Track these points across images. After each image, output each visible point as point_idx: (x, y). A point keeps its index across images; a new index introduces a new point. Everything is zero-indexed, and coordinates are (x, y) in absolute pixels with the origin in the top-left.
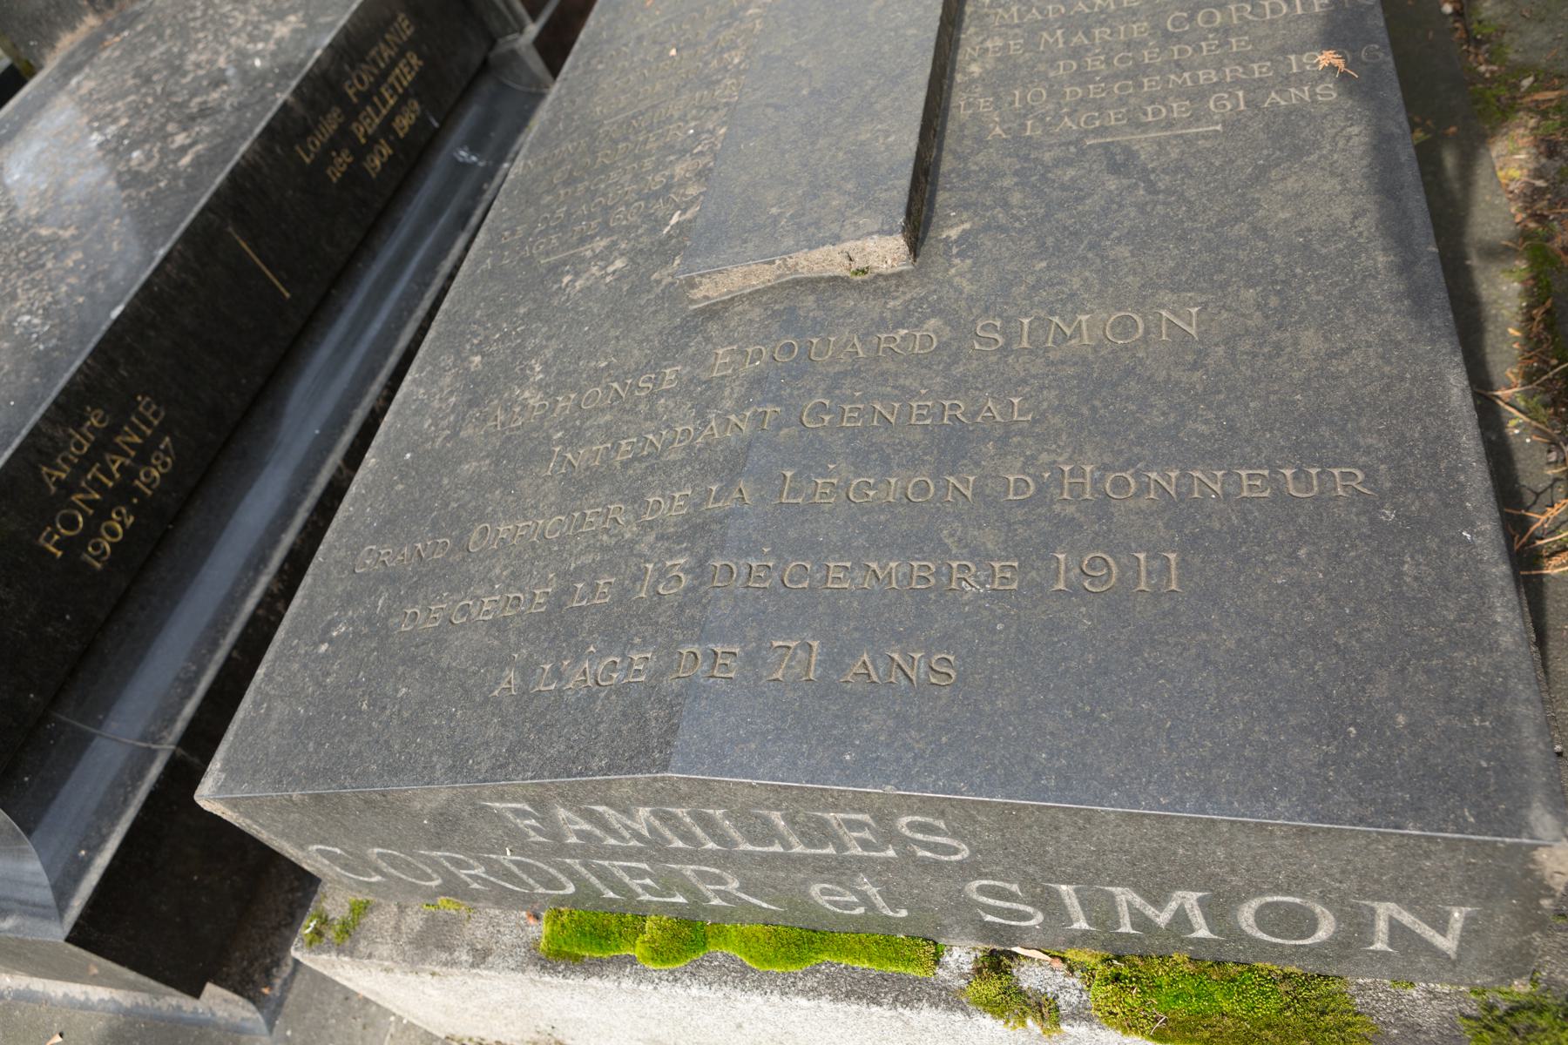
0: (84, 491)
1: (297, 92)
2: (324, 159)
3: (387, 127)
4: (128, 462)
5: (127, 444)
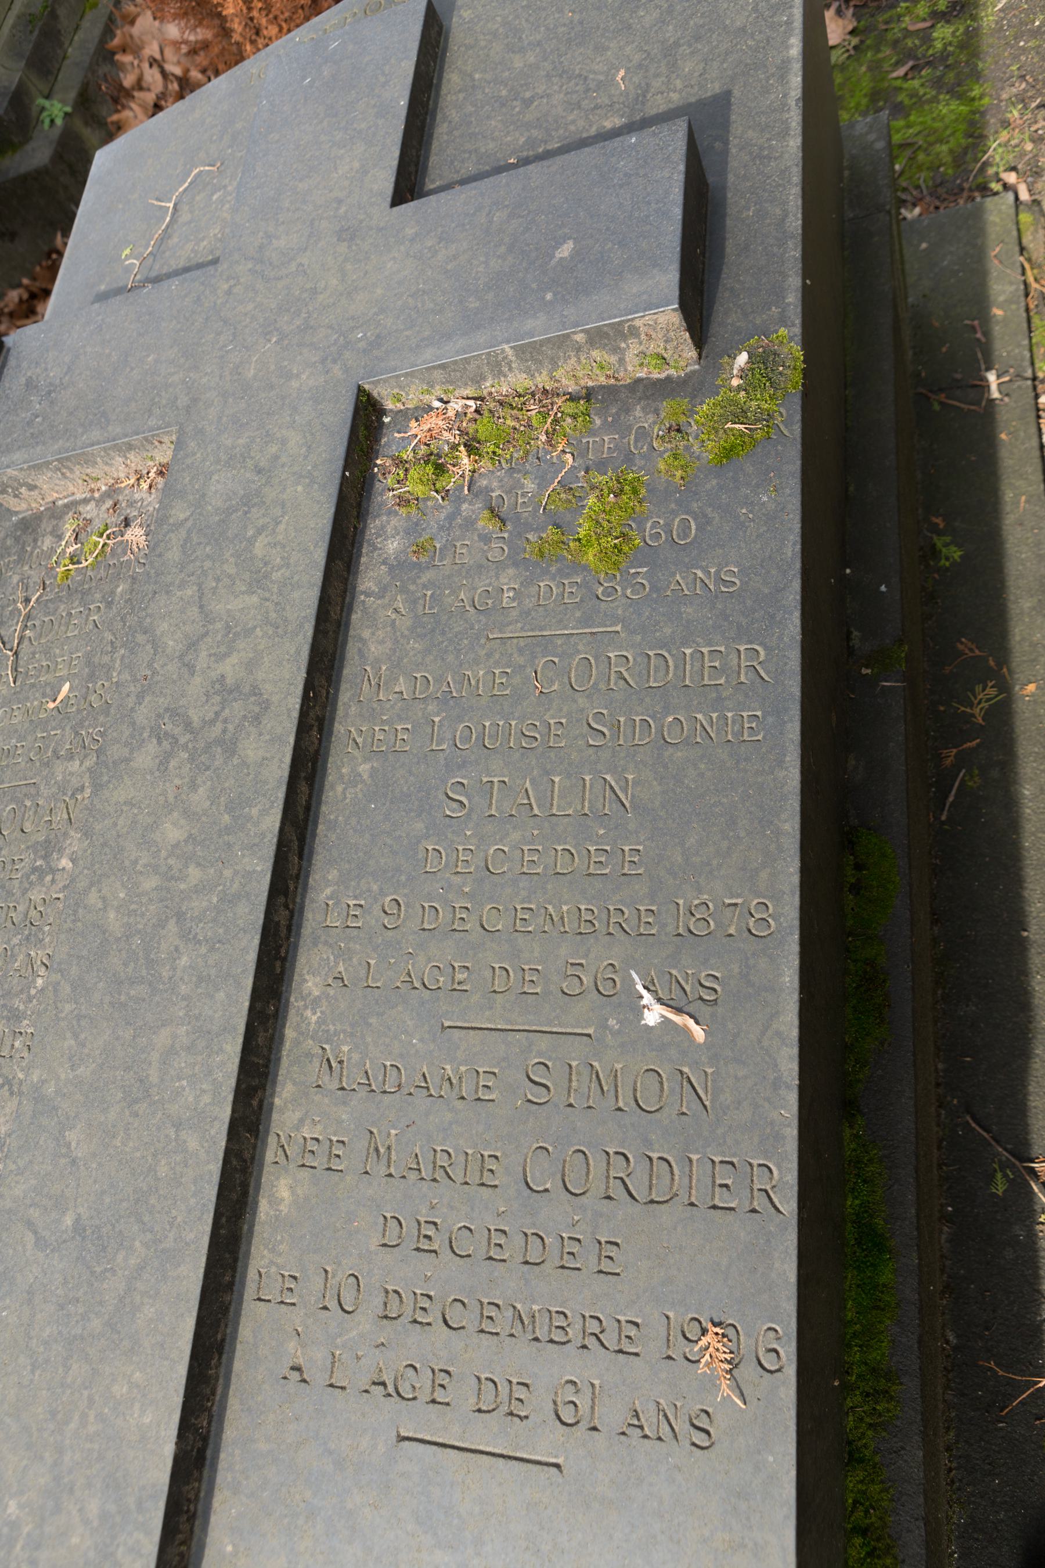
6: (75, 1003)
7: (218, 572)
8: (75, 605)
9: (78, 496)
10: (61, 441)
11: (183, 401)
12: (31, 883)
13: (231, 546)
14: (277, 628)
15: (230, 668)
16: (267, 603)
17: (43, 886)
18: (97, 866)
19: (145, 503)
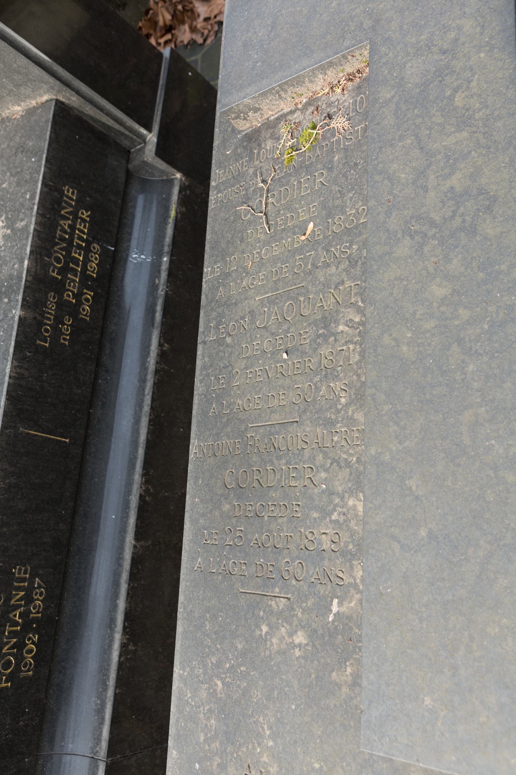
0: (7, 643)
1: (25, 305)
2: (57, 332)
3: (85, 277)
4: (70, 222)
5: (17, 600)
6: (391, 404)
7: (429, 124)
8: (302, 176)
9: (286, 110)
10: (279, 73)
11: (368, 23)
12: (319, 344)
13: (435, 105)
14: (489, 148)
15: (456, 181)
16: (476, 135)
17: (329, 344)
18: (384, 321)
19: (341, 102)
